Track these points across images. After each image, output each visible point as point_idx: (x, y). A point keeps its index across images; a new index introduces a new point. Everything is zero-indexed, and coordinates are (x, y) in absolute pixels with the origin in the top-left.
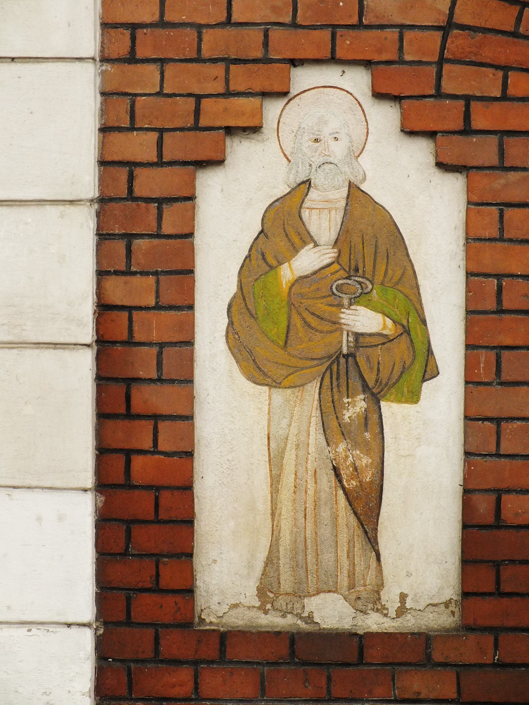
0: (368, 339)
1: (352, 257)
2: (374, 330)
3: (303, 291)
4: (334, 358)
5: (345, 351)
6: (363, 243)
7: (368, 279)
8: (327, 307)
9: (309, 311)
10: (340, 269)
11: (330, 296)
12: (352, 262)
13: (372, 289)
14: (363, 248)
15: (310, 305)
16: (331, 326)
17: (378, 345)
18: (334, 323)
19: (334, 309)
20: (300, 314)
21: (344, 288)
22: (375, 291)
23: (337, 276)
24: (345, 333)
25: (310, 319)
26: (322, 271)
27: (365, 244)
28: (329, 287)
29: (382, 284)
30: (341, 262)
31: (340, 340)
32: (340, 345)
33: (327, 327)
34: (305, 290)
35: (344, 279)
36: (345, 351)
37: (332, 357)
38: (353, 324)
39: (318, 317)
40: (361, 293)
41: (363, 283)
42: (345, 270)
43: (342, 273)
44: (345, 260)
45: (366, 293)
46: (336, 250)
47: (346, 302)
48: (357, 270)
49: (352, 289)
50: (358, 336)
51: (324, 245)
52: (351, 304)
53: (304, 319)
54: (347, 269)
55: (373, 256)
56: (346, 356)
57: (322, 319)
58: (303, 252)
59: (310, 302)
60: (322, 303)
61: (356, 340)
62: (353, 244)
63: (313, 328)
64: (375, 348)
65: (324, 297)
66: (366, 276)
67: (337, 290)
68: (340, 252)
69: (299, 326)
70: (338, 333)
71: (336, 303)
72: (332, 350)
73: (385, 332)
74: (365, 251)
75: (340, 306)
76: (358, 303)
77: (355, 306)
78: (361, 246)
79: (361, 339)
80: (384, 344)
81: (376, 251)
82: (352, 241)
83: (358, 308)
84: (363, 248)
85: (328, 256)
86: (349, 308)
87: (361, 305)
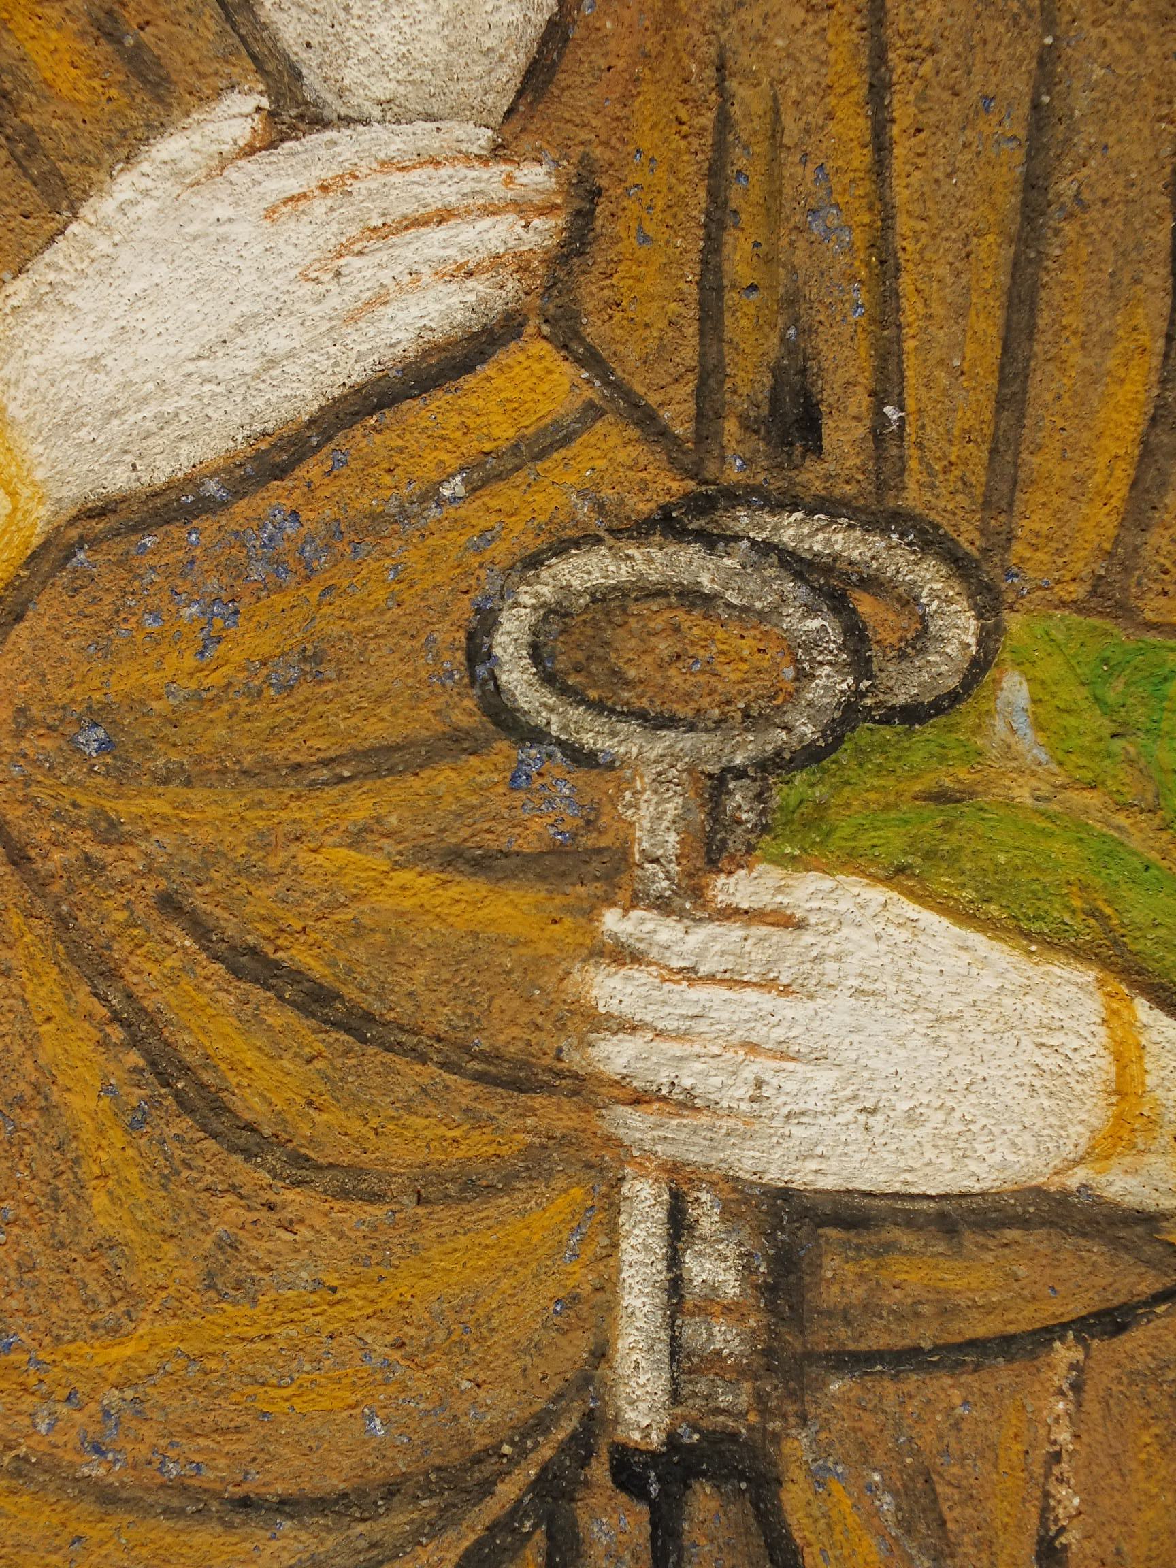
0: (918, 1272)
1: (739, 259)
2: (990, 1163)
3: (129, 678)
4: (508, 1491)
5: (642, 1405)
6: (878, 90)
7: (930, 540)
8: (421, 884)
9: (200, 929)
10: (592, 413)
11: (458, 744)
12: (740, 321)
13: (979, 668)
14: (881, 146)
15: (211, 856)
16: (477, 1121)
17: (1047, 1335)
18: (516, 1078)
19: (509, 909)
20: (103, 973)
21: (639, 654)
22: (1014, 688)
23: (555, 491)
24: (644, 1199)
25: (217, 1024)
26: (362, 441)
27: (902, 107)
28: (450, 635)
29: (1107, 598)
30: (594, 329)
31: (582, 1278)
32: (577, 1348)
33: (423, 1126)
34: (160, 673)
35: (640, 530)
36: (642, 1405)
37: (486, 1488)
38: (737, 1094)
39: (316, 1000)
40: (851, 713)
41: (872, 583)
42: (645, 420)
43: (612, 462)
44: (644, 300)
45: (912, 715)
46: (535, 177)
47: (655, 821)
48: (795, 421)
49: (738, 661)
50: (796, 1230)
51: (394, 112)
52: (713, 849)
53: (137, 1026)
54: (677, 414)
55: (993, 252)
56: (659, 1477)
57: (359, 1025)
58: (130, 200)
59: (216, 818)
60: (357, 839)
61: (782, 1282)
62: (749, 100)
63: (250, 1141)
64: (1004, 1374)
65: (381, 761)
66: (912, 498)
67: (549, 679)
68: (584, 201)
69: (82, 1104)
70: (554, 1207)
71: (535, 831)
72: (495, 1407)
73: (1122, 1185)
74: (901, 193)
75: (590, 866)
76: (809, 839)
77: (769, 875)
78: (854, 124)
79: (839, 1275)
80: (1112, 1321)
81: (1034, 186)
82: (746, 59)
83: (808, 891)
84: (881, 146)
85: (434, 244)
86: (688, 899)
87: (851, 861)
